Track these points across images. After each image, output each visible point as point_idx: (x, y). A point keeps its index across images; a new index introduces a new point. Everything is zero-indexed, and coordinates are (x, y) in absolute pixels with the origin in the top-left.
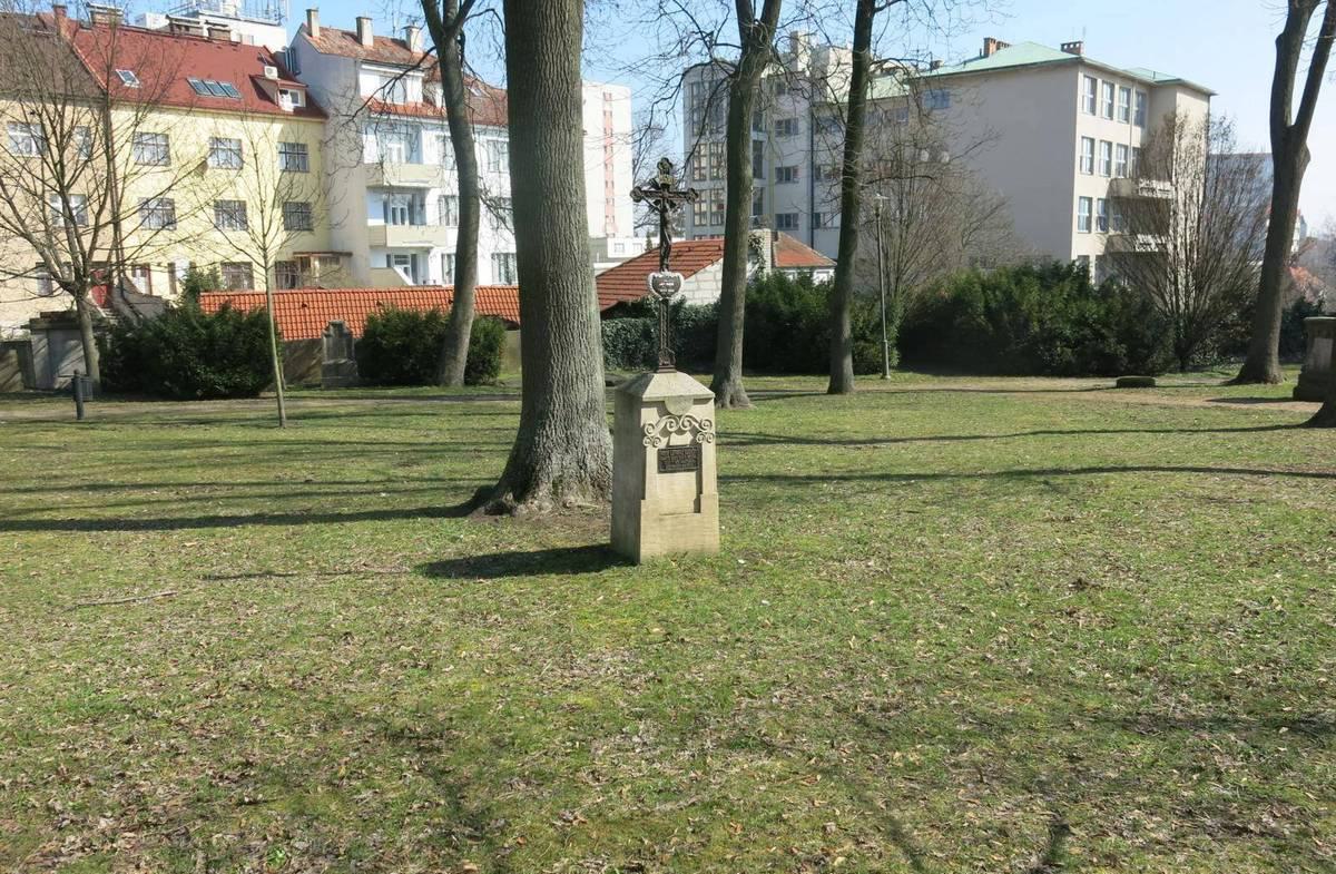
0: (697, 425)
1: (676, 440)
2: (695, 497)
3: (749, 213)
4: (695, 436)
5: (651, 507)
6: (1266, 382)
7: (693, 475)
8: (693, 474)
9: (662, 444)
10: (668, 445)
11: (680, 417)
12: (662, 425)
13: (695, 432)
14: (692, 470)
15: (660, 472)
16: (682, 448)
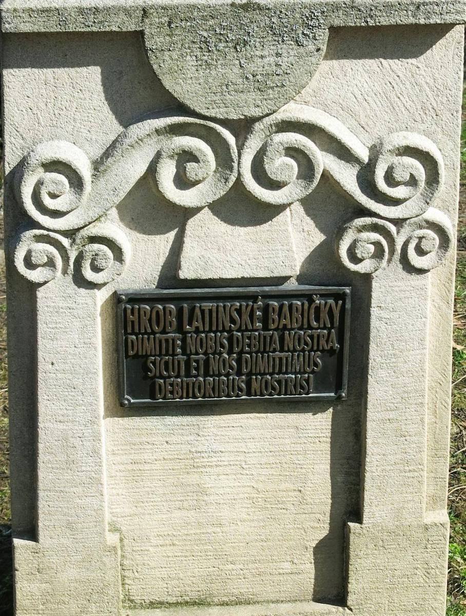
0: (347, 177)
1: (220, 252)
2: (322, 530)
3: (273, 343)
4: (335, 233)
5: (70, 574)
6: (302, 199)
7: (316, 428)
8: (319, 425)
9: (140, 262)
10: (170, 273)
11: (243, 128)
12: (132, 168)
13: (333, 209)
14: (315, 406)
15: (121, 406)
16: (252, 298)
